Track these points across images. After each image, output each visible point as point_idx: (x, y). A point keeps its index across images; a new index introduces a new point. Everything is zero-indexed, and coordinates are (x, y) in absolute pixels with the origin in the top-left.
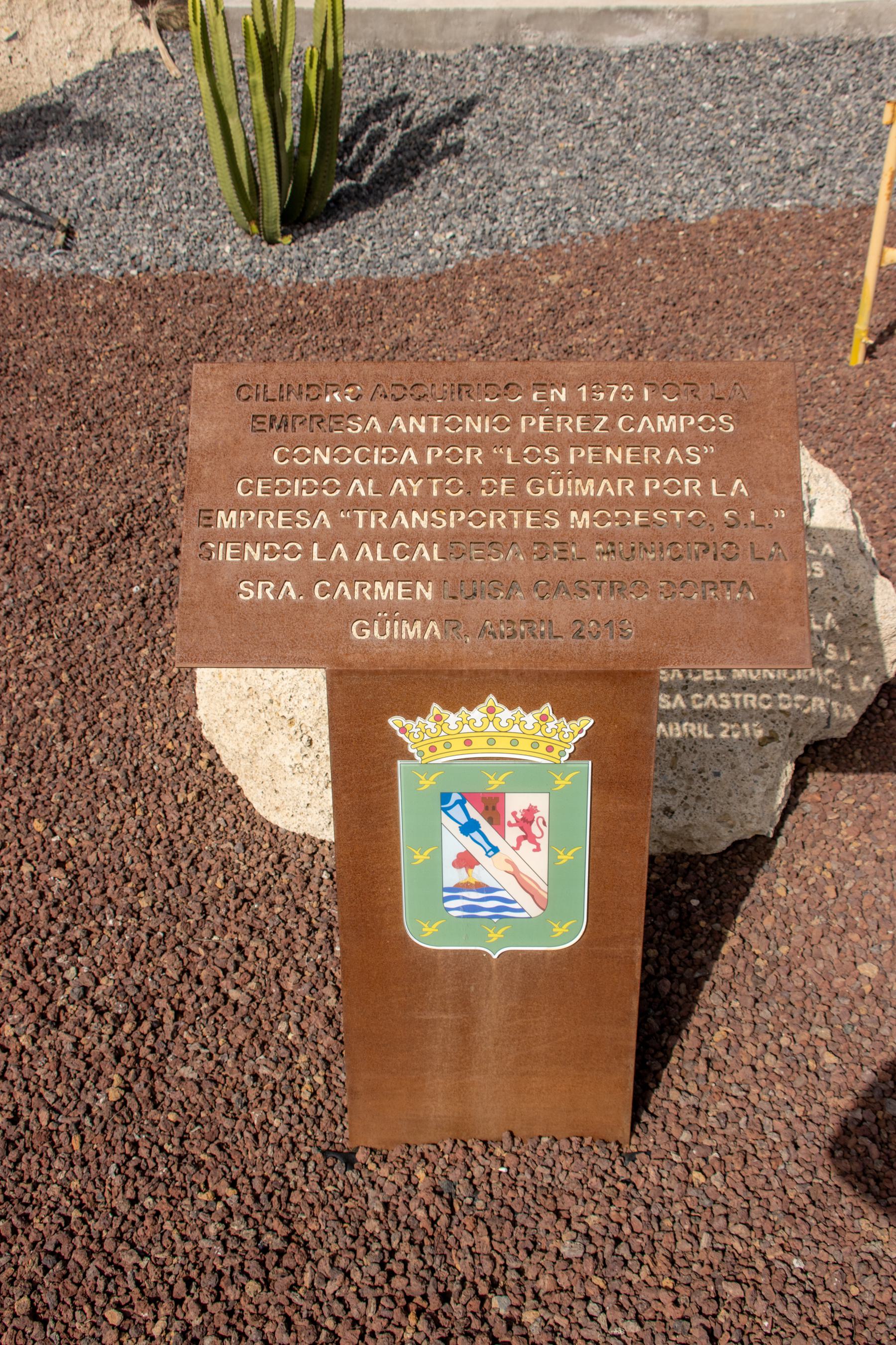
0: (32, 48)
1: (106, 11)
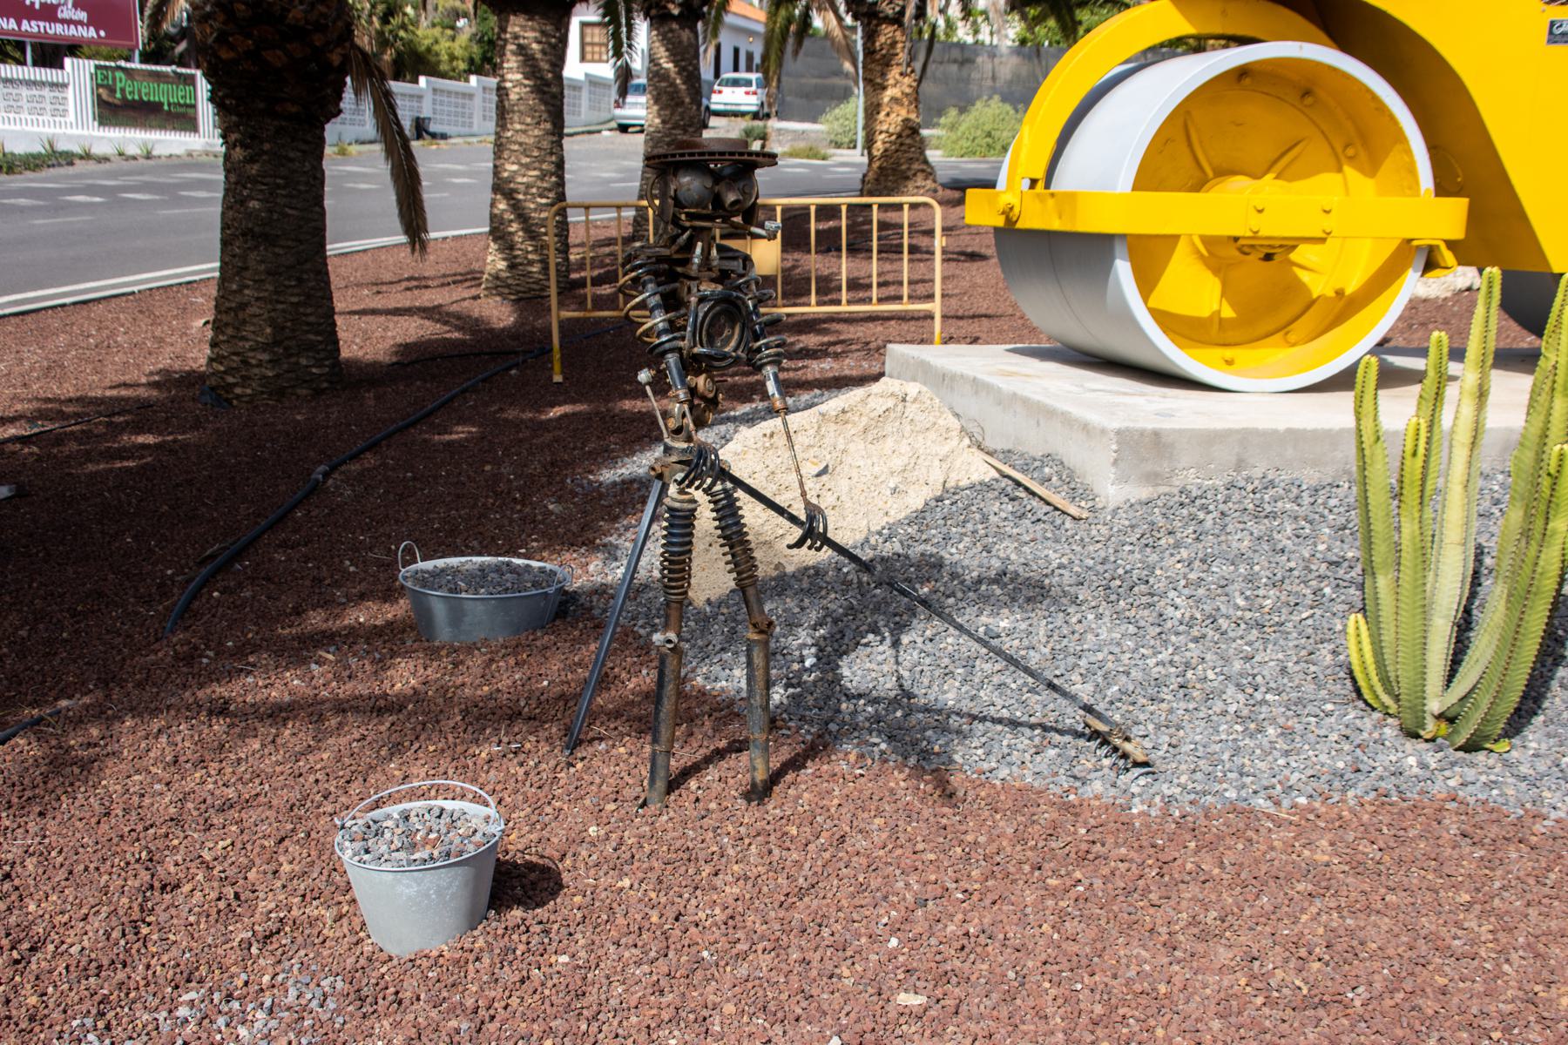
0: (844, 484)
1: (932, 435)
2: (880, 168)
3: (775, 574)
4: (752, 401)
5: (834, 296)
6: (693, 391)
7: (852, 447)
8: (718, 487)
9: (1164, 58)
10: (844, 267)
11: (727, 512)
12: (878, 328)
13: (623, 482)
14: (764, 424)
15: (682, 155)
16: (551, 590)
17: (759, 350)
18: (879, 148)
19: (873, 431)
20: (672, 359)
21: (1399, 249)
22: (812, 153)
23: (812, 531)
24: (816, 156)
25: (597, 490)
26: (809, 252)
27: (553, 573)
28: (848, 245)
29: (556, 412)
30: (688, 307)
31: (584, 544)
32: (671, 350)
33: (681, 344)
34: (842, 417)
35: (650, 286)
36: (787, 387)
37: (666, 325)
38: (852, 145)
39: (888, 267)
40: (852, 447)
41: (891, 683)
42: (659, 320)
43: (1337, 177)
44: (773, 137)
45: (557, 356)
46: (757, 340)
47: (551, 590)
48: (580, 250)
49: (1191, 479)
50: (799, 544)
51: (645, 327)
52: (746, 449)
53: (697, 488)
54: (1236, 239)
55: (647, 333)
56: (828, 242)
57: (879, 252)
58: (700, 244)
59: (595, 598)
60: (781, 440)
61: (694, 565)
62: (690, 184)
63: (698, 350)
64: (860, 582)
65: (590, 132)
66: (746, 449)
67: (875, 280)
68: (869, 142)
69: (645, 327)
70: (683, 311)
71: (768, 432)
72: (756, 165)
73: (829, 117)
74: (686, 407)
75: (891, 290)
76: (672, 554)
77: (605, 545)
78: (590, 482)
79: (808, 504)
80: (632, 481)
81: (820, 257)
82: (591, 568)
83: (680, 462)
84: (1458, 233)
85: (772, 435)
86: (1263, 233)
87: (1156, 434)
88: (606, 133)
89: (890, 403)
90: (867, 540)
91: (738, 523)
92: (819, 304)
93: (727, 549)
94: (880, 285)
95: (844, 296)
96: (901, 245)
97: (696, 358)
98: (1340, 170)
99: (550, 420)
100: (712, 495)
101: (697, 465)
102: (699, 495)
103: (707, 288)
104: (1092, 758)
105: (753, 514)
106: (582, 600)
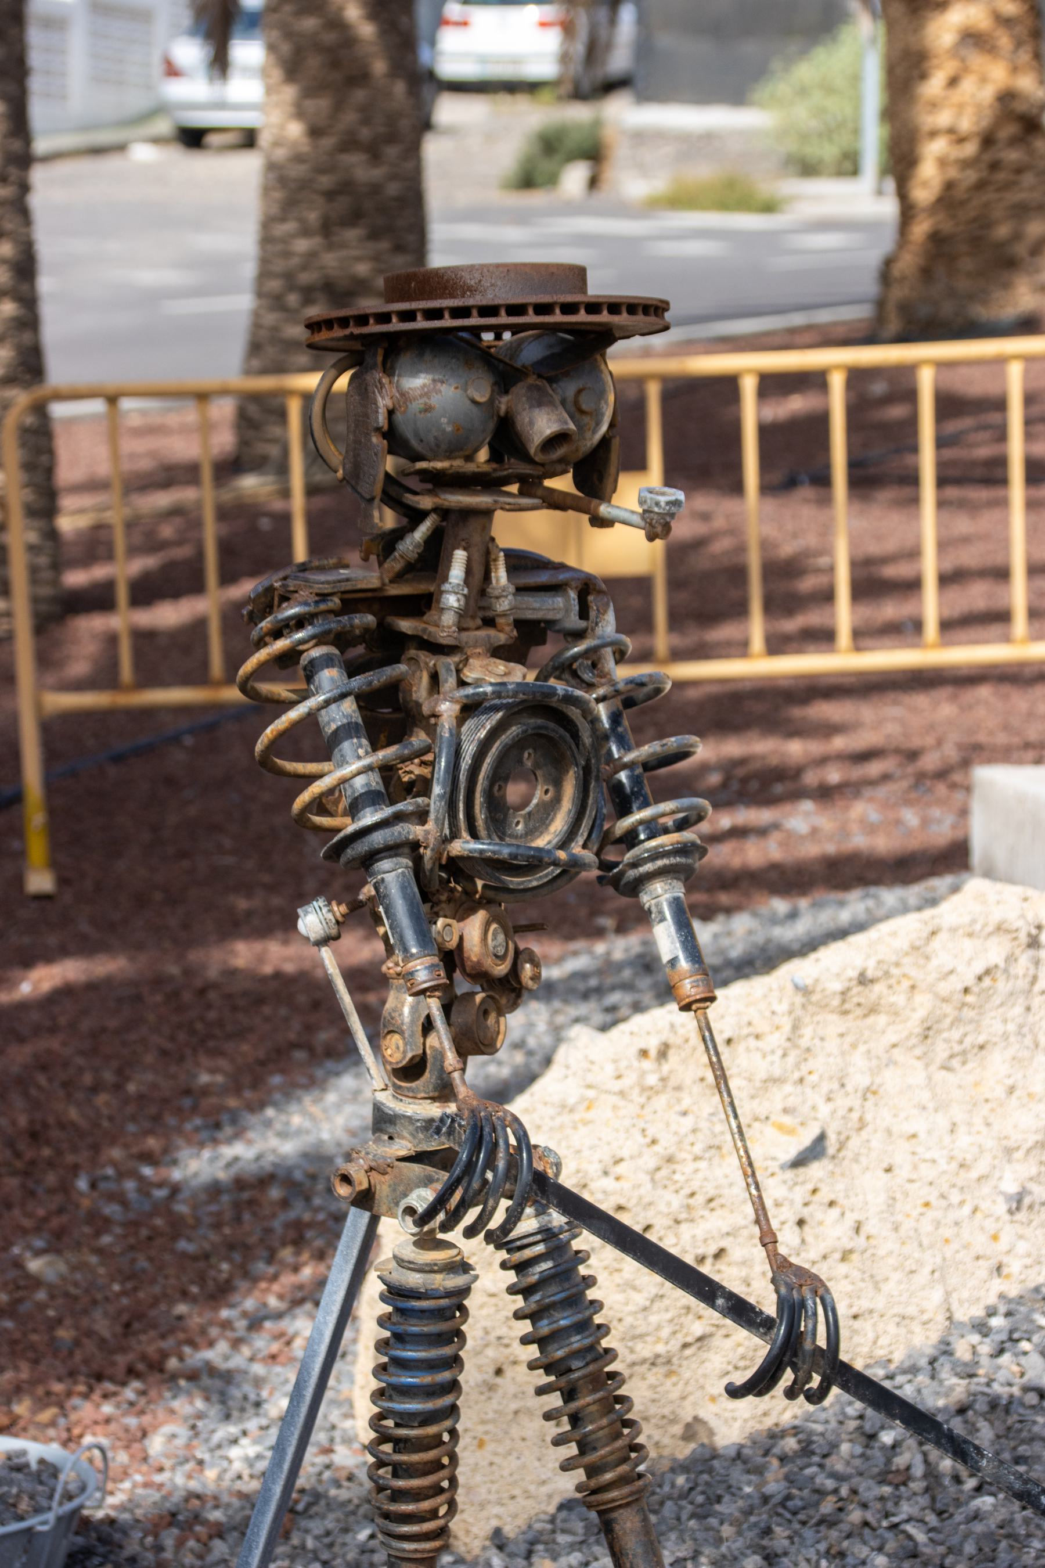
0: (868, 1190)
2: (936, 238)
3: (685, 1451)
4: (599, 933)
5: (812, 618)
6: (451, 959)
7: (890, 1080)
8: (528, 1224)
10: (840, 532)
11: (554, 1293)
12: (940, 708)
13: (240, 1183)
14: (639, 1021)
15: (408, 316)
16: (43, 1523)
17: (630, 839)
18: (929, 176)
19: (951, 1032)
20: (393, 874)
22: (733, 195)
23: (796, 1346)
25: (164, 1207)
26: (737, 488)
27: (49, 1470)
28: (853, 465)
29: (37, 982)
30: (432, 731)
31: (132, 1372)
32: (391, 850)
33: (415, 831)
34: (858, 994)
35: (329, 678)
36: (711, 891)
37: (374, 781)
38: (849, 166)
39: (963, 524)
40: (890, 1080)
42: (354, 766)
44: (620, 152)
46: (624, 811)
47: (43, 1523)
48: (86, 500)
50: (760, 1384)
51: (317, 788)
52: (598, 1096)
53: (470, 1232)
55: (320, 805)
56: (795, 459)
57: (942, 482)
58: (460, 556)
59: (169, 1538)
60: (691, 1065)
61: (464, 1449)
62: (430, 393)
63: (463, 846)
64: (931, 1473)
65: (97, 151)
66: (598, 1096)
67: (929, 567)
68: (901, 161)
69: (317, 788)
70: (419, 738)
71: (653, 1045)
72: (606, 337)
73: (781, 87)
74: (434, 1005)
75: (976, 596)
76: (404, 1419)
77: (193, 1376)
78: (145, 1186)
79: (782, 1269)
80: (265, 1180)
81: (771, 505)
82: (156, 1445)
83: (418, 1158)
85: (663, 1053)
88: (143, 153)
89: (995, 952)
90: (945, 1349)
91: (584, 1326)
92: (776, 645)
93: (555, 1400)
94: (947, 580)
95: (844, 614)
96: (1001, 462)
97: (457, 867)
99: (23, 1006)
100: (511, 1247)
101: (470, 1167)
102: (478, 1251)
103: (488, 674)
105: (617, 1284)
106: (132, 1547)
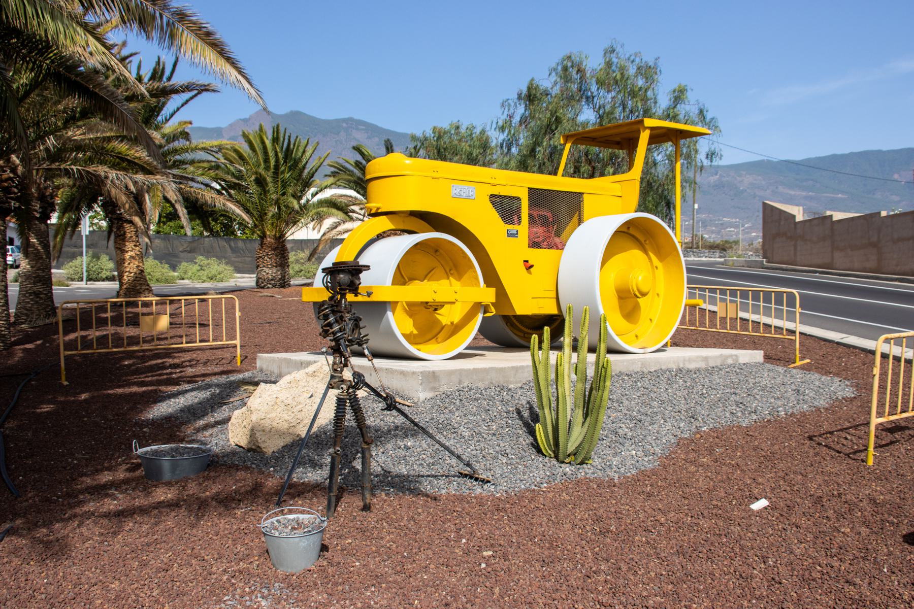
9: (396, 234)
21: (473, 306)
24: (63, 285)
41: (379, 469)
43: (447, 281)
45: (63, 372)
49: (444, 388)
54: (427, 303)
84: (494, 301)
86: (437, 300)
87: (434, 372)
98: (448, 278)
104: (469, 483)
